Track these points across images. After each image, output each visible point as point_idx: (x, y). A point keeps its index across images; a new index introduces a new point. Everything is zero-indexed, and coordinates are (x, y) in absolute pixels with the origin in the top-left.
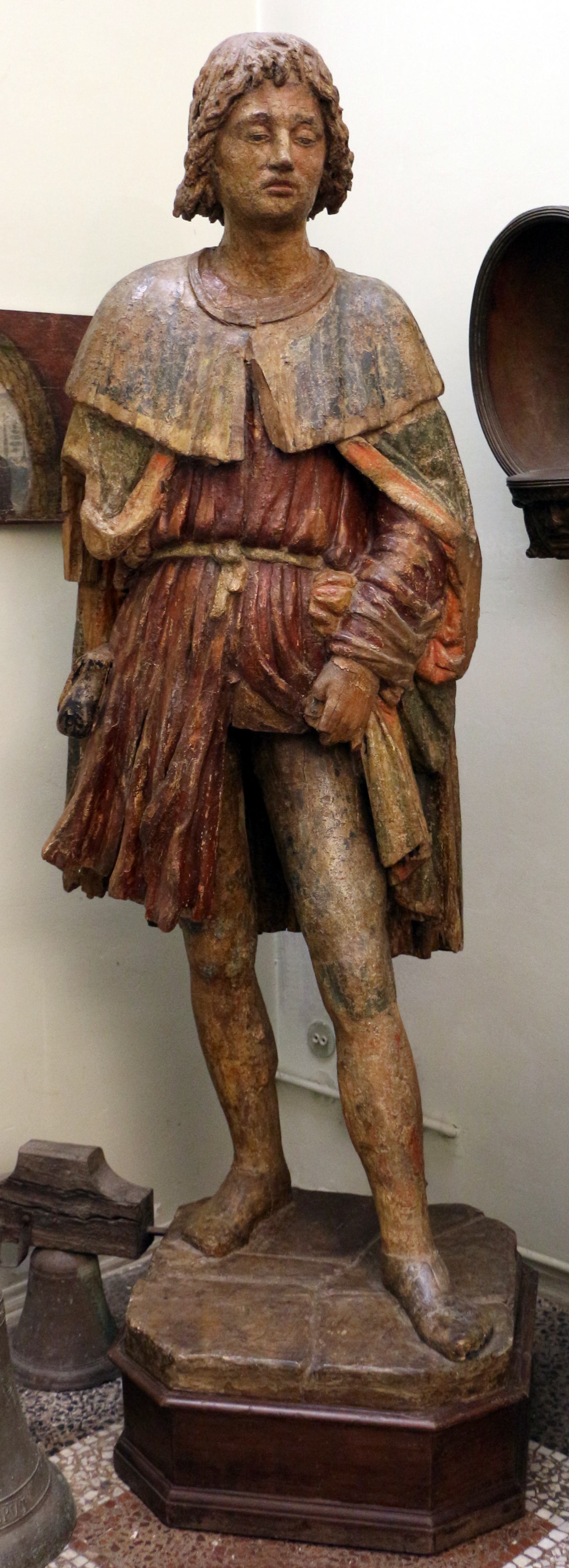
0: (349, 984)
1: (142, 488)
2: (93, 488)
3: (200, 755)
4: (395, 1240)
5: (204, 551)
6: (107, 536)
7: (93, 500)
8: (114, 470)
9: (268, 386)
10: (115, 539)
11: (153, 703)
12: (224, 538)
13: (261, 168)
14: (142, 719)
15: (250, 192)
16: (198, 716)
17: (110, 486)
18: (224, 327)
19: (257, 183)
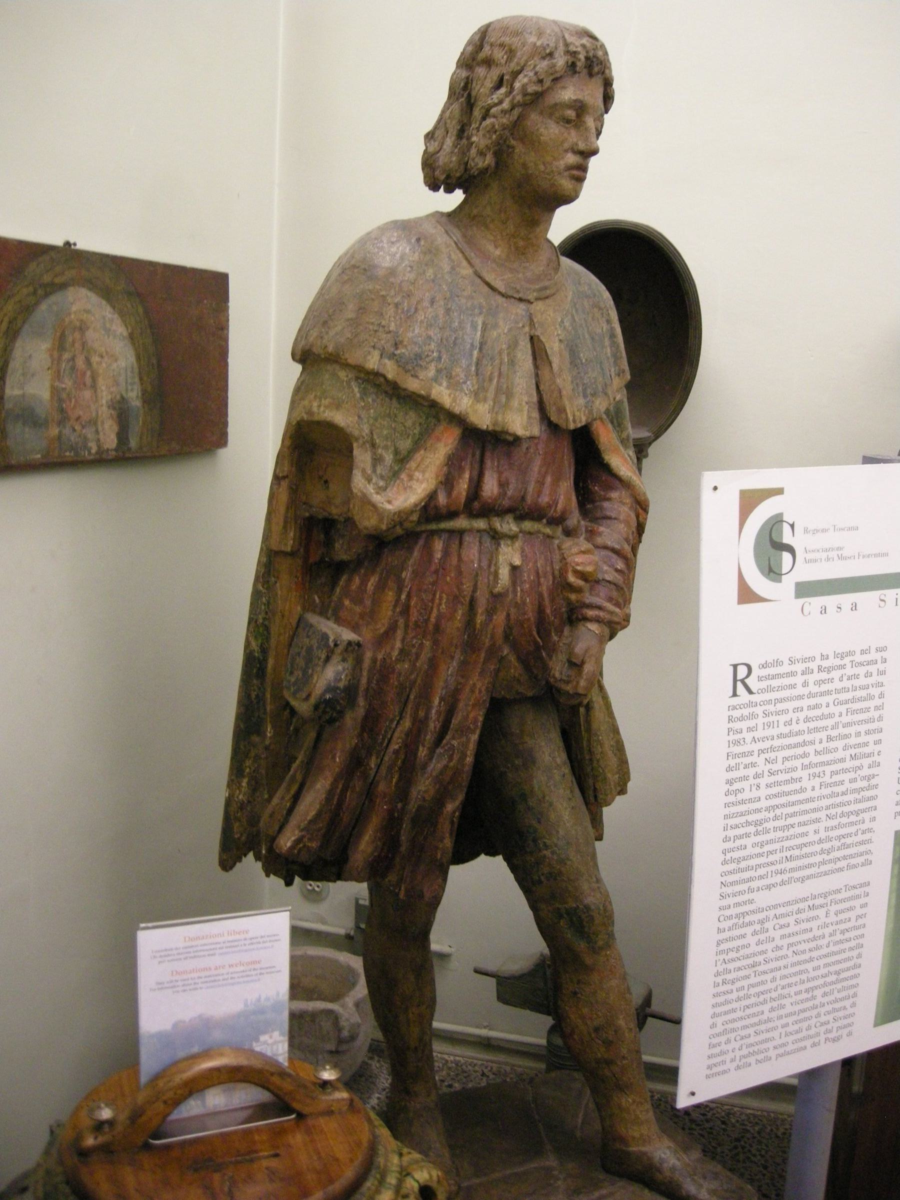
0: (597, 922)
1: (422, 459)
2: (362, 457)
3: (478, 732)
4: (636, 1134)
5: (481, 524)
6: (385, 510)
7: (364, 471)
8: (387, 439)
9: (550, 363)
10: (395, 513)
11: (419, 681)
12: (502, 512)
13: (566, 151)
14: (406, 698)
15: (552, 171)
16: (477, 692)
17: (381, 456)
18: (504, 299)
19: (562, 164)
